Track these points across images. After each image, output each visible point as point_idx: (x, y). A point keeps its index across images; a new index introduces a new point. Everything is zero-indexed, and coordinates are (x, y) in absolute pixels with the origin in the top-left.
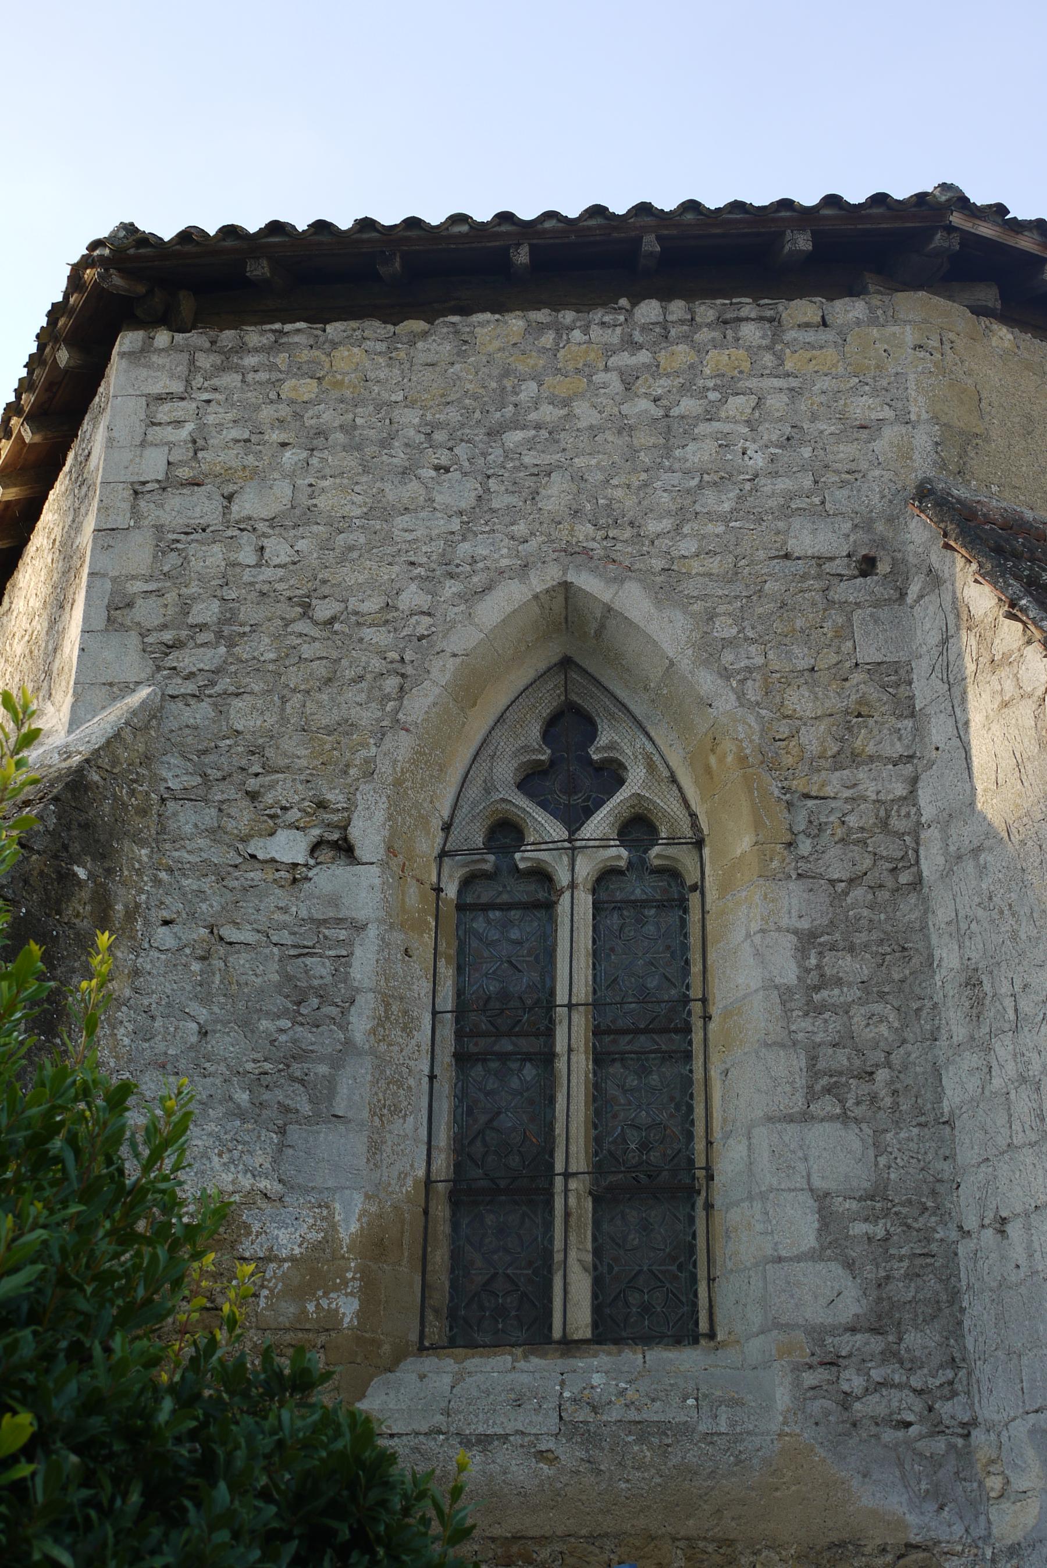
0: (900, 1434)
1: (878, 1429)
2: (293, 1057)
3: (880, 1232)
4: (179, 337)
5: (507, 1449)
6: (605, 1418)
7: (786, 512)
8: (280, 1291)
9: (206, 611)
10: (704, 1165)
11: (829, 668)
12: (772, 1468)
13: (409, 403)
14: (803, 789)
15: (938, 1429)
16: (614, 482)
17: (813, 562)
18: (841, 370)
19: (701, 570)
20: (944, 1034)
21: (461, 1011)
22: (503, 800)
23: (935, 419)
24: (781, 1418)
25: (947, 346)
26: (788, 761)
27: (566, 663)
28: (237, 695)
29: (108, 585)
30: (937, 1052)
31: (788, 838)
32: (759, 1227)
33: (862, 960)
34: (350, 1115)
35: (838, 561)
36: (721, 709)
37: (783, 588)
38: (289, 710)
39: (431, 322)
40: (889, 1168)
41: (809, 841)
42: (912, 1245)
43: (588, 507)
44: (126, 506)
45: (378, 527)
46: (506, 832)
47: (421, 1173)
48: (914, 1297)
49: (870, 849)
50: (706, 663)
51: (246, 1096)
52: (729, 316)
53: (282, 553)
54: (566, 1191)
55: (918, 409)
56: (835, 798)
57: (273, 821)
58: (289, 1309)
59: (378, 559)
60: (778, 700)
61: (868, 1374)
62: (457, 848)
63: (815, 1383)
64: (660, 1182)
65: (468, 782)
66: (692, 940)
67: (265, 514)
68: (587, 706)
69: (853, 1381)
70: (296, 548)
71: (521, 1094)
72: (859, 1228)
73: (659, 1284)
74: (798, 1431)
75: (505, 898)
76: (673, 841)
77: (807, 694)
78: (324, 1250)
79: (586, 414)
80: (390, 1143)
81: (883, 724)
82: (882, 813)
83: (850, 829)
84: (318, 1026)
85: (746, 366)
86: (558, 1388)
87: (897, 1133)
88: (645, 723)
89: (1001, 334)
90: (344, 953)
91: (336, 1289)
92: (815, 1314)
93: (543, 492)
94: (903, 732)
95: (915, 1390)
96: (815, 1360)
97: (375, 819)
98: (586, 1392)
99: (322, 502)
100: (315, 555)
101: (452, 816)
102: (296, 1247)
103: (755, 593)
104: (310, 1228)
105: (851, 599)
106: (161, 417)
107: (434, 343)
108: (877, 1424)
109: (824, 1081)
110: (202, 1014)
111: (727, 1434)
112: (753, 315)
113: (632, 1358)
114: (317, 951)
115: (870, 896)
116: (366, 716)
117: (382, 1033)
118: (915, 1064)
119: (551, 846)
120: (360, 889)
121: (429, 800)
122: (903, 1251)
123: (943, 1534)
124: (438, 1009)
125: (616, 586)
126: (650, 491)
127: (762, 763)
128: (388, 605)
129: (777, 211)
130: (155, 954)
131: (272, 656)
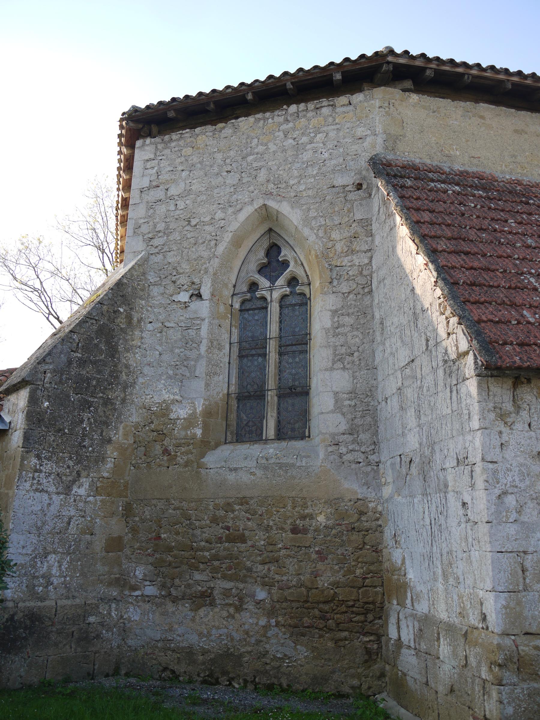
3: (353, 403)
4: (153, 140)
7: (333, 171)
9: (161, 226)
13: (219, 151)
15: (369, 464)
16: (280, 169)
18: (354, 120)
19: (306, 195)
20: (376, 341)
21: (240, 343)
23: (385, 132)
25: (391, 106)
27: (270, 230)
29: (134, 222)
30: (374, 346)
31: (330, 280)
34: (200, 376)
39: (226, 123)
41: (336, 281)
43: (272, 178)
44: (138, 196)
46: (253, 286)
47: (226, 392)
50: (306, 226)
51: (172, 372)
52: (318, 106)
55: (379, 129)
57: (179, 289)
58: (183, 433)
60: (329, 235)
63: (331, 450)
64: (296, 393)
67: (177, 193)
68: (279, 243)
72: (347, 403)
75: (254, 307)
76: (303, 284)
79: (272, 147)
82: (360, 269)
85: (323, 123)
89: (413, 97)
91: (196, 427)
92: (332, 430)
93: (258, 175)
96: (333, 443)
99: (193, 188)
104: (189, 410)
105: (353, 199)
106: (148, 167)
107: (226, 130)
109: (338, 357)
110: (160, 349)
112: (326, 105)
113: (284, 444)
115: (355, 297)
116: (205, 254)
120: (203, 308)
122: (360, 409)
123: (369, 495)
125: (279, 203)
126: (291, 170)
129: (329, 67)
130: (147, 332)
131: (179, 238)
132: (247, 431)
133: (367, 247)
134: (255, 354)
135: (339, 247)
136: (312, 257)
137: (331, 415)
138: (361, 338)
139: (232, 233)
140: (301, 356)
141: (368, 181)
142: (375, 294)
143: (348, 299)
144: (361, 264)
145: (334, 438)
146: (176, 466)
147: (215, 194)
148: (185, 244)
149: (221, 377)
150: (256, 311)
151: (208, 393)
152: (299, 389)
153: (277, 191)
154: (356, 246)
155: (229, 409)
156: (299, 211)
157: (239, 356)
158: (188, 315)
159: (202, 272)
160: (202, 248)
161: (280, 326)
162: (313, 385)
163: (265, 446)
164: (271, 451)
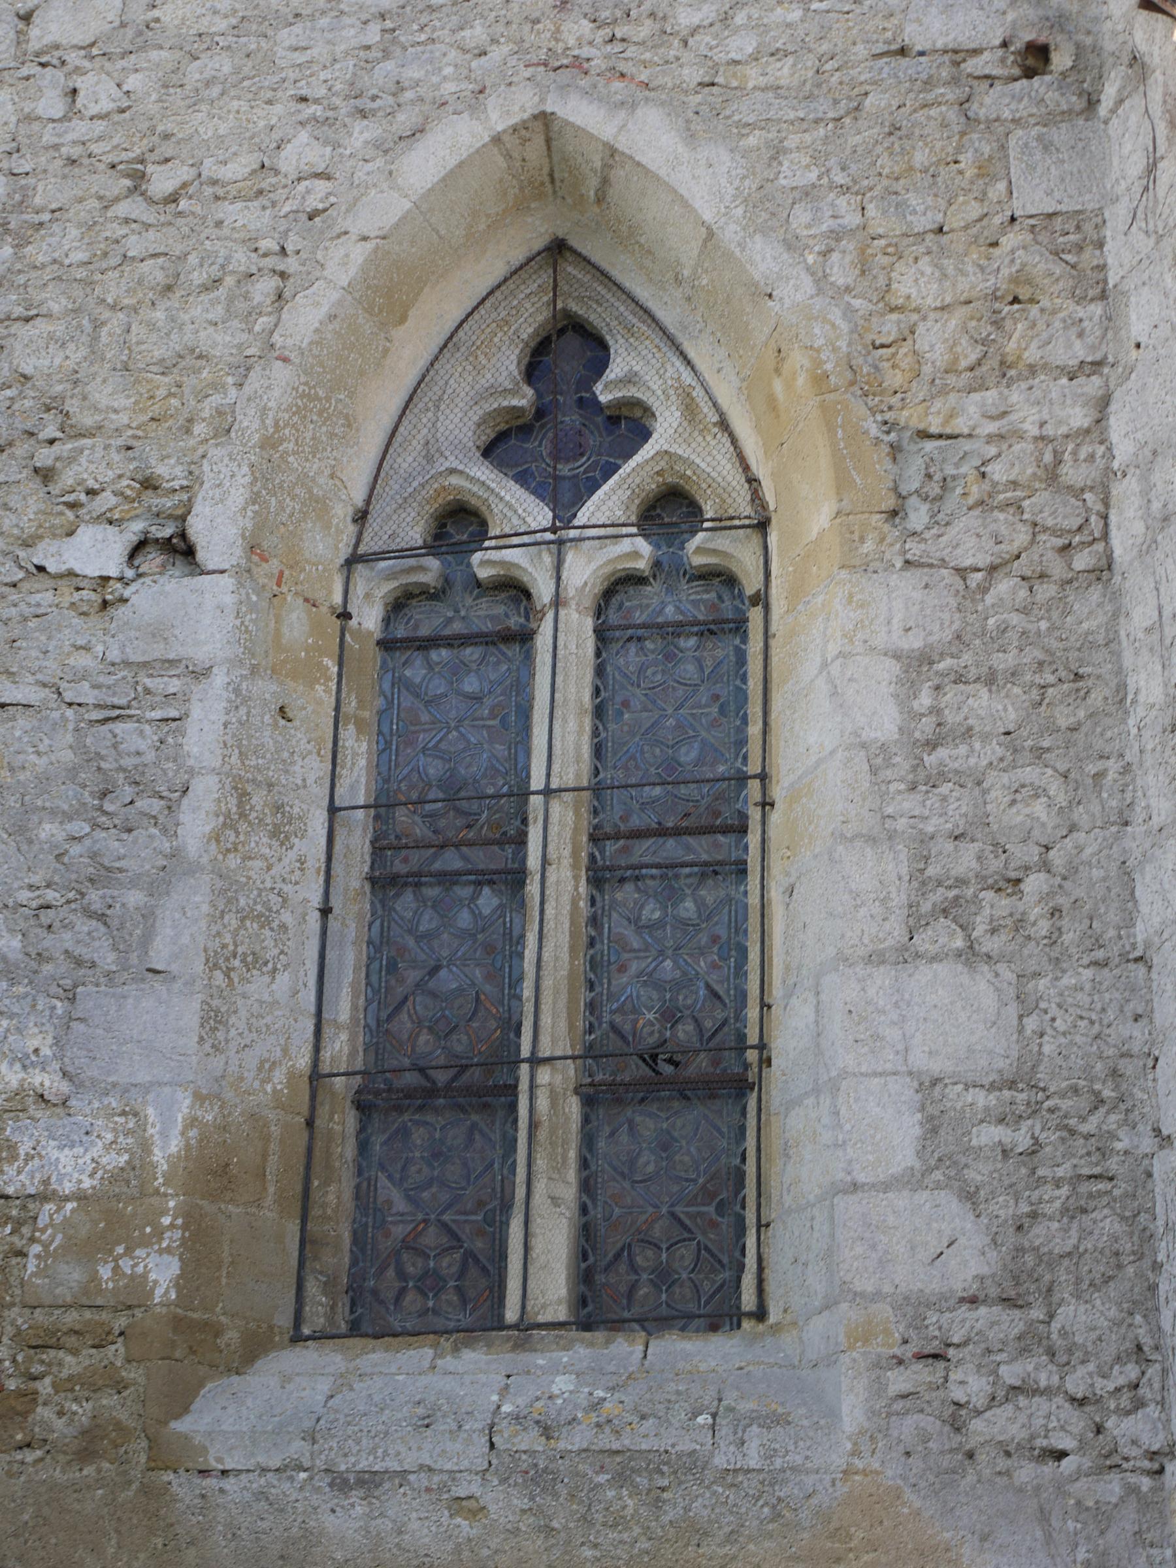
0: (1049, 1468)
1: (1009, 1462)
2: (91, 880)
3: (1022, 1139)
5: (405, 1494)
6: (562, 1445)
8: (60, 1246)
10: (756, 1042)
11: (966, 228)
12: (832, 1526)
14: (916, 424)
15: (1110, 1462)
17: (946, 58)
19: (762, 81)
20: (1139, 815)
21: (382, 806)
22: (452, 471)
24: (849, 1446)
26: (895, 379)
27: (558, 249)
28: (27, 320)
30: (1128, 843)
31: (890, 503)
32: (827, 1137)
33: (1007, 696)
34: (174, 968)
35: (986, 56)
36: (787, 301)
37: (895, 103)
38: (104, 338)
40: (1042, 1035)
41: (924, 508)
42: (1075, 1161)
45: (253, 46)
46: (458, 524)
47: (303, 1062)
48: (1077, 1247)
49: (1025, 517)
50: (764, 231)
53: (103, 96)
54: (532, 1087)
56: (970, 436)
57: (75, 509)
58: (72, 1275)
59: (251, 96)
60: (882, 281)
61: (995, 1373)
62: (385, 548)
64: (689, 1073)
65: (395, 444)
66: (751, 683)
67: (82, 37)
68: (596, 317)
69: (969, 1384)
70: (125, 88)
71: (474, 936)
72: (989, 1135)
73: (686, 1235)
74: (876, 1466)
75: (457, 627)
76: (724, 524)
77: (929, 270)
78: (128, 1182)
80: (243, 1013)
81: (1054, 312)
82: (1048, 458)
83: (995, 484)
84: (130, 831)
86: (495, 1398)
87: (1057, 979)
88: (681, 338)
90: (174, 713)
91: (145, 1242)
92: (910, 1276)
94: (1086, 324)
95: (1073, 1400)
97: (229, 502)
98: (539, 1404)
100: (154, 97)
101: (368, 502)
102: (85, 1178)
103: (848, 113)
104: (108, 1148)
105: (1007, 114)
108: (1008, 1454)
109: (939, 896)
111: (761, 1471)
113: (626, 1349)
114: (132, 712)
115: (1023, 593)
116: (222, 342)
117: (232, 838)
118: (1089, 864)
119: (526, 539)
120: (199, 614)
121: (327, 472)
122: (1060, 1172)
124: (337, 803)
125: (622, 114)
127: (852, 383)
128: (263, 166)
132: (418, 1276)
133: (1080, 352)
134: (458, 873)
135: (936, 341)
136: (789, 386)
137: (901, 1200)
138: (1062, 800)
139: (369, 246)
140: (710, 894)
141: (1080, 37)
142: (1135, 584)
143: (989, 599)
144: (1049, 430)
145: (918, 1323)
146: (30, 1456)
147: (280, 52)
148: (114, 287)
149: (284, 979)
150: (471, 653)
151: (217, 1062)
152: (701, 1064)
153: (607, 57)
154: (1020, 341)
155: (317, 1153)
156: (725, 156)
157: (372, 880)
158: (117, 641)
159: (199, 429)
160: (200, 309)
161: (595, 733)
162: (791, 1034)
163: (524, 1358)
164: (562, 1384)
